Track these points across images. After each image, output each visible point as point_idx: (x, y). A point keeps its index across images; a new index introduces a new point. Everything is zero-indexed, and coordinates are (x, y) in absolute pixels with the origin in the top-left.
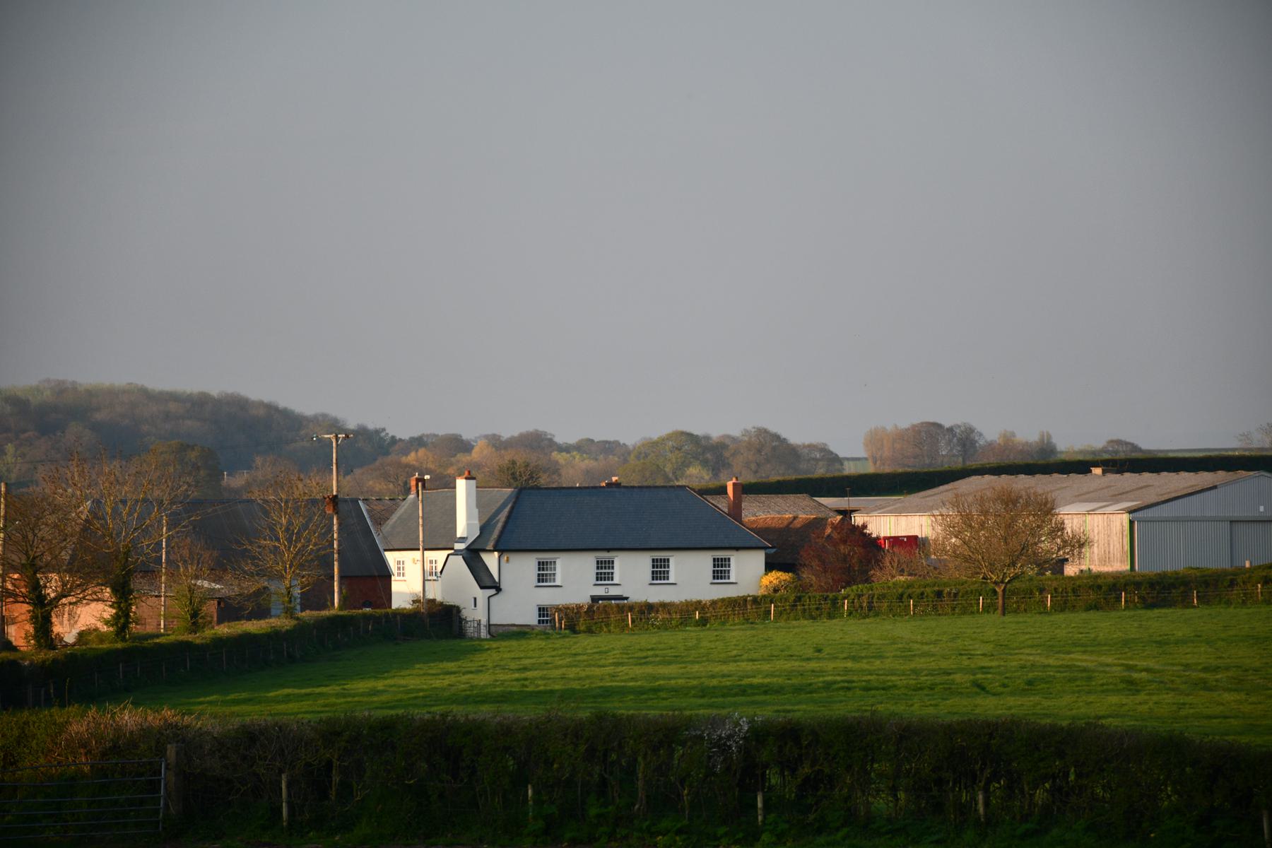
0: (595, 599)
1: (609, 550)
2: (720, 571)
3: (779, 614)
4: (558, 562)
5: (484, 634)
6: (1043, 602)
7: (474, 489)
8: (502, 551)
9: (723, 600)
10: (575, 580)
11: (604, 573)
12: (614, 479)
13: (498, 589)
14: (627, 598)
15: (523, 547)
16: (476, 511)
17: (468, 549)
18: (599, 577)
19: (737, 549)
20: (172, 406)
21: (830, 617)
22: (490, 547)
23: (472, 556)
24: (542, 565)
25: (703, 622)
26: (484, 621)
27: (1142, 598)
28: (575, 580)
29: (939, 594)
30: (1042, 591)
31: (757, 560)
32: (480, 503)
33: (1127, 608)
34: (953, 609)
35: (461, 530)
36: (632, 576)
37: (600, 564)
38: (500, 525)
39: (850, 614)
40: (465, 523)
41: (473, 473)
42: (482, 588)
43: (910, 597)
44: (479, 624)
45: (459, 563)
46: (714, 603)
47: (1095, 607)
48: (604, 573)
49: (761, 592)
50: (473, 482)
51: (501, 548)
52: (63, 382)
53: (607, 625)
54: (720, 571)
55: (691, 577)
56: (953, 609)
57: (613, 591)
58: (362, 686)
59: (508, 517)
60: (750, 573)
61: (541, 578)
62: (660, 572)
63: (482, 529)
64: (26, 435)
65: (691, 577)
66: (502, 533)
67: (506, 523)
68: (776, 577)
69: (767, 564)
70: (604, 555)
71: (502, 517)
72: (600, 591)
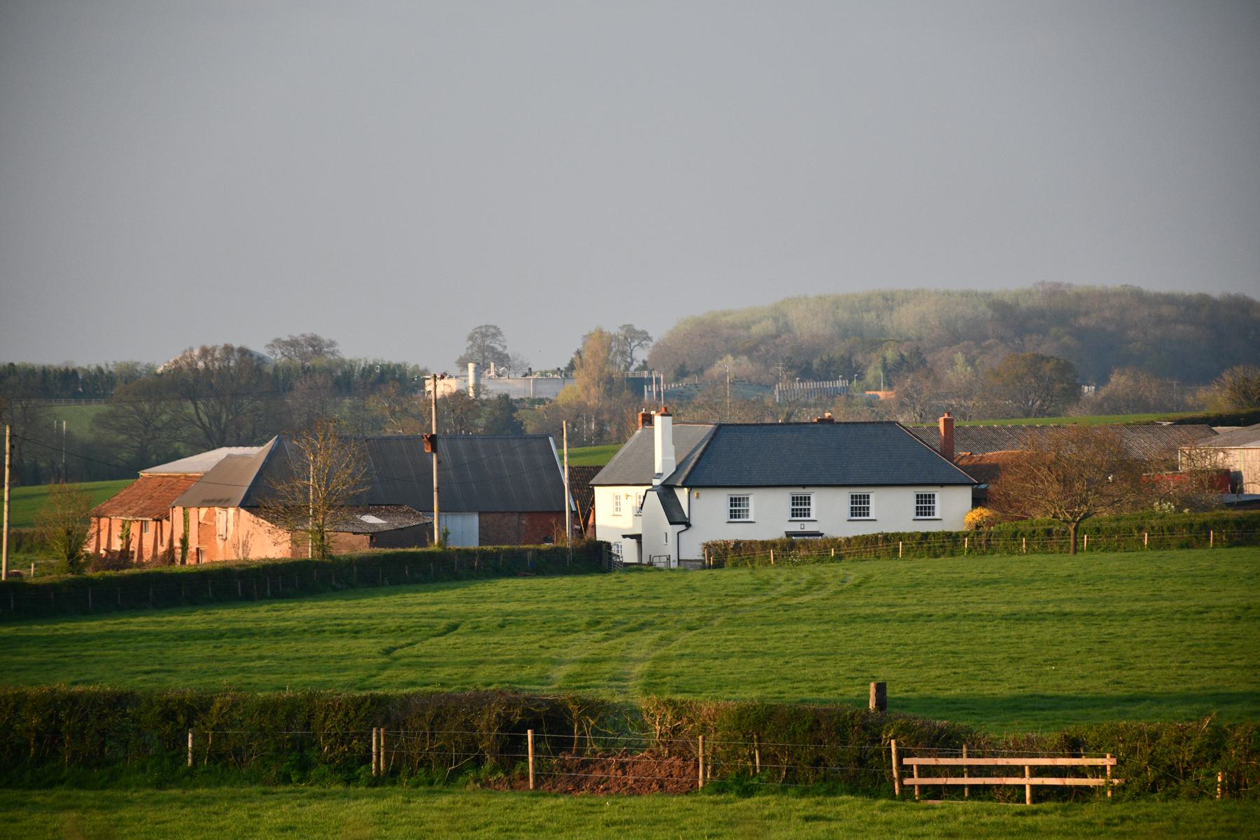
0: (789, 534)
1: (804, 486)
2: (924, 507)
3: (906, 552)
4: (751, 498)
5: (674, 565)
6: (1141, 541)
7: (670, 426)
8: (691, 487)
9: (856, 538)
10: (769, 515)
11: (800, 508)
12: (827, 415)
13: (688, 525)
14: (821, 535)
15: (952, 481)
16: (672, 448)
17: (662, 485)
18: (919, 511)
19: (942, 485)
20: (1166, 311)
21: (952, 554)
22: (679, 484)
23: (667, 492)
24: (734, 501)
25: (839, 558)
26: (674, 557)
27: (1229, 537)
28: (769, 515)
29: (1049, 533)
30: (1140, 529)
31: (963, 496)
32: (676, 439)
33: (1215, 546)
34: (1061, 547)
35: (658, 468)
36: (830, 513)
37: (795, 500)
38: (694, 461)
39: (970, 551)
40: (663, 460)
41: (670, 411)
42: (671, 523)
43: (1023, 535)
44: (669, 559)
45: (654, 497)
46: (848, 540)
47: (1186, 546)
48: (800, 508)
49: (964, 529)
50: (670, 418)
51: (689, 484)
52: (1059, 285)
53: (752, 562)
54: (924, 507)
55: (892, 510)
56: (1061, 547)
57: (809, 527)
58: (71, 625)
59: (702, 454)
60: (955, 509)
61: (733, 514)
62: (859, 508)
63: (677, 469)
64: (987, 343)
65: (892, 510)
66: (690, 473)
67: (699, 459)
68: (983, 512)
69: (973, 499)
70: (800, 492)
71: (697, 454)
72: (796, 527)
